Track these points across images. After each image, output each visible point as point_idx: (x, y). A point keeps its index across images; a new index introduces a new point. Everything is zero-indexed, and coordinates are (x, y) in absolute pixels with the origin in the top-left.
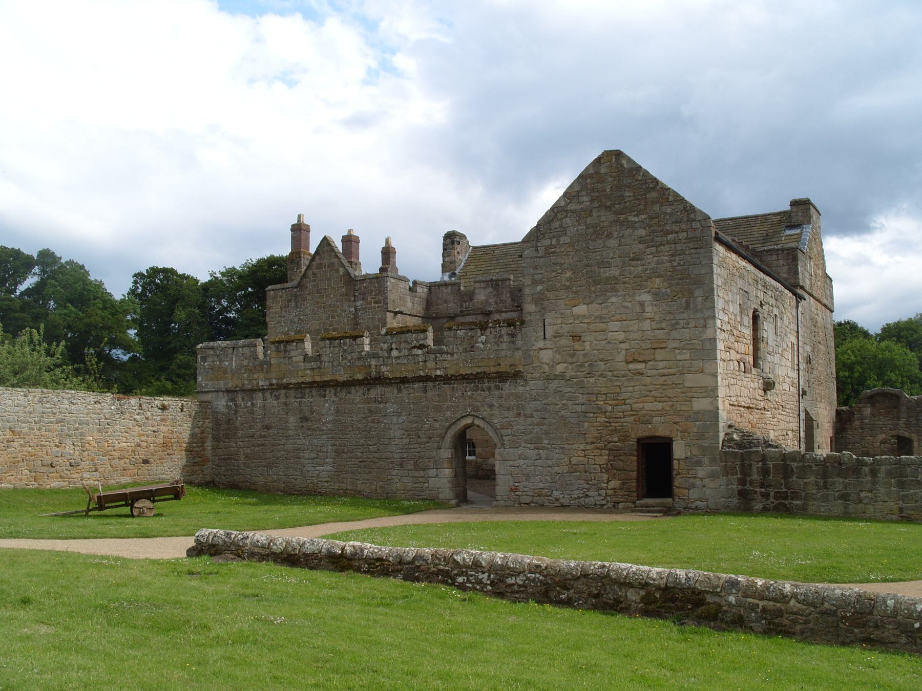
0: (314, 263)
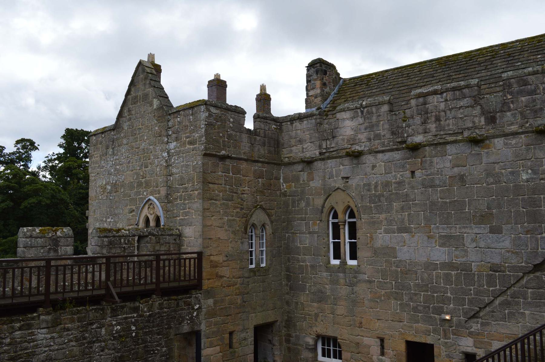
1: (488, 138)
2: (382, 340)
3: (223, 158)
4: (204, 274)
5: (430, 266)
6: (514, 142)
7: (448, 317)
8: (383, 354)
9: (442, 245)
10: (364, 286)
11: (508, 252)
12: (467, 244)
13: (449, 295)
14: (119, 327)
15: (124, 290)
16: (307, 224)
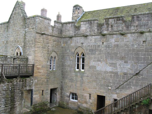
0: (13, 12)
1: (126, 34)
2: (90, 95)
3: (43, 34)
4: (35, 72)
5: (106, 72)
6: (133, 35)
7: (110, 88)
8: (90, 99)
9: (110, 66)
10: (86, 78)
11: (129, 69)
12: (117, 66)
13: (111, 81)
14: (5, 87)
15: (7, 75)
16: (69, 57)
